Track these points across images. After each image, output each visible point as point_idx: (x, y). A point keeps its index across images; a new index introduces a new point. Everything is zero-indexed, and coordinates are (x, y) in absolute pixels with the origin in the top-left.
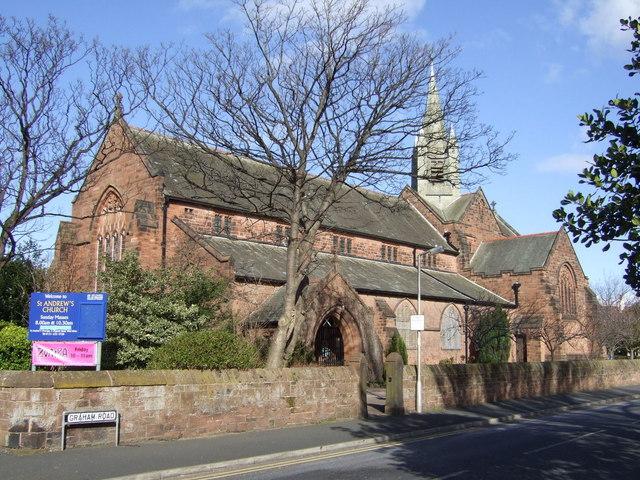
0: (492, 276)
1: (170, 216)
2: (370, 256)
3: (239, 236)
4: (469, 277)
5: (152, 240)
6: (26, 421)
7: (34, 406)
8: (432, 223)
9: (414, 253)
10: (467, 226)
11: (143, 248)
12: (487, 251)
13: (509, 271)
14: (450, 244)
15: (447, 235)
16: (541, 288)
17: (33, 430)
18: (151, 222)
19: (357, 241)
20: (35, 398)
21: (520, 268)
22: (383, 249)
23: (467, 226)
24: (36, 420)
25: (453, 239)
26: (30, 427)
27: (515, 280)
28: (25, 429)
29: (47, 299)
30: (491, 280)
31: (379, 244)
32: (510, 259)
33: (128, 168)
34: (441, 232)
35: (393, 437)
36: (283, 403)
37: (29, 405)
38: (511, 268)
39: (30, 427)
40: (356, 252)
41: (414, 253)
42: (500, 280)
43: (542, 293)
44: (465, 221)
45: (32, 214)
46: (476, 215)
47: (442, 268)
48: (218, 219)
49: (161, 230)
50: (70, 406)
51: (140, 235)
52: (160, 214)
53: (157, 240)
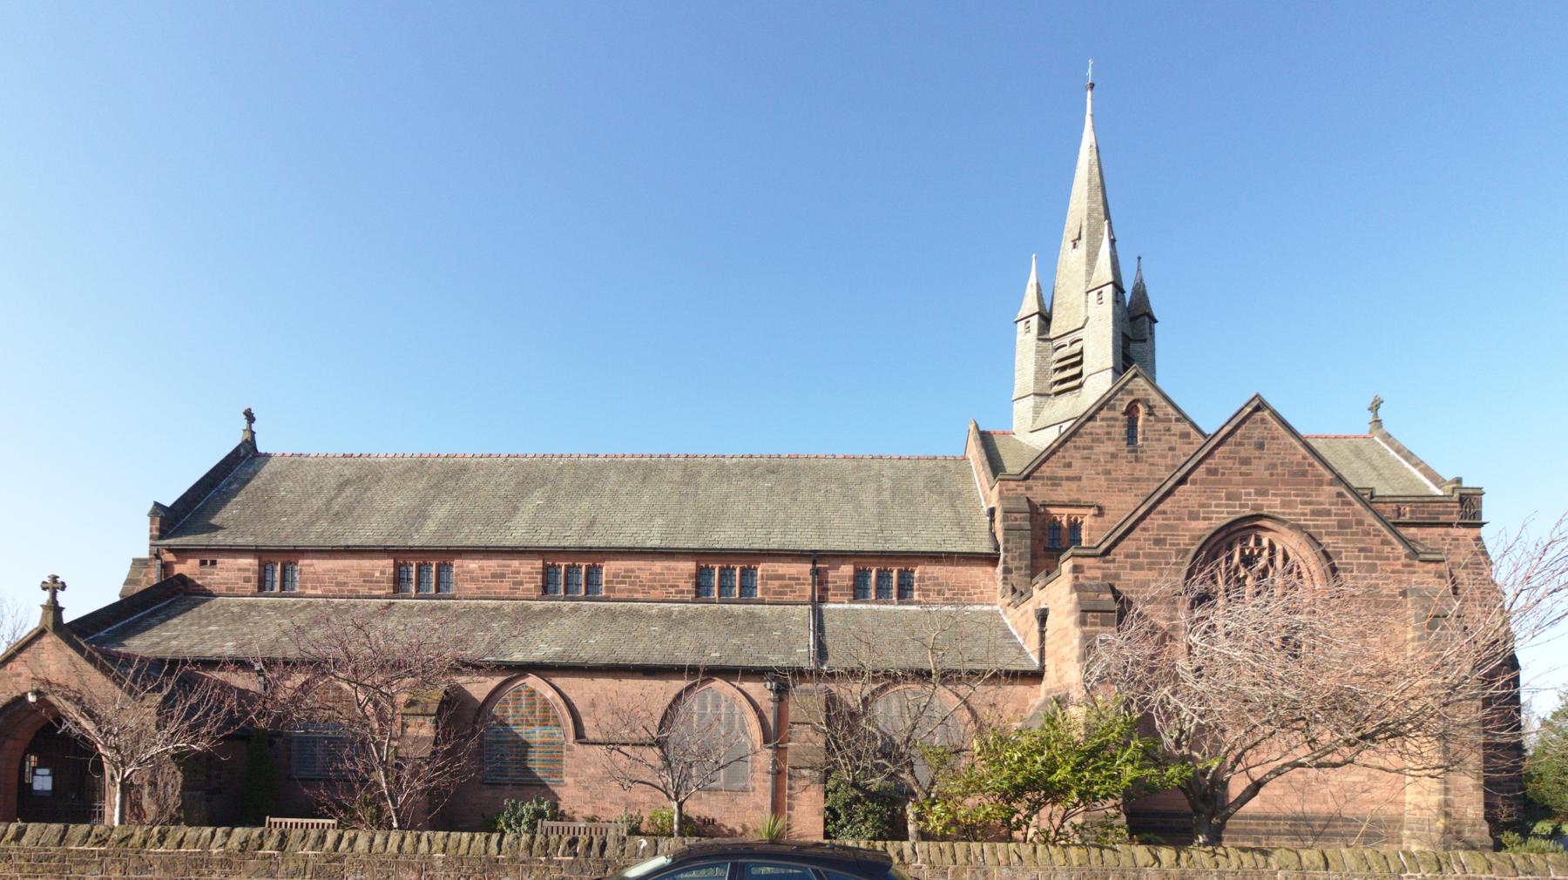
2: (654, 594)
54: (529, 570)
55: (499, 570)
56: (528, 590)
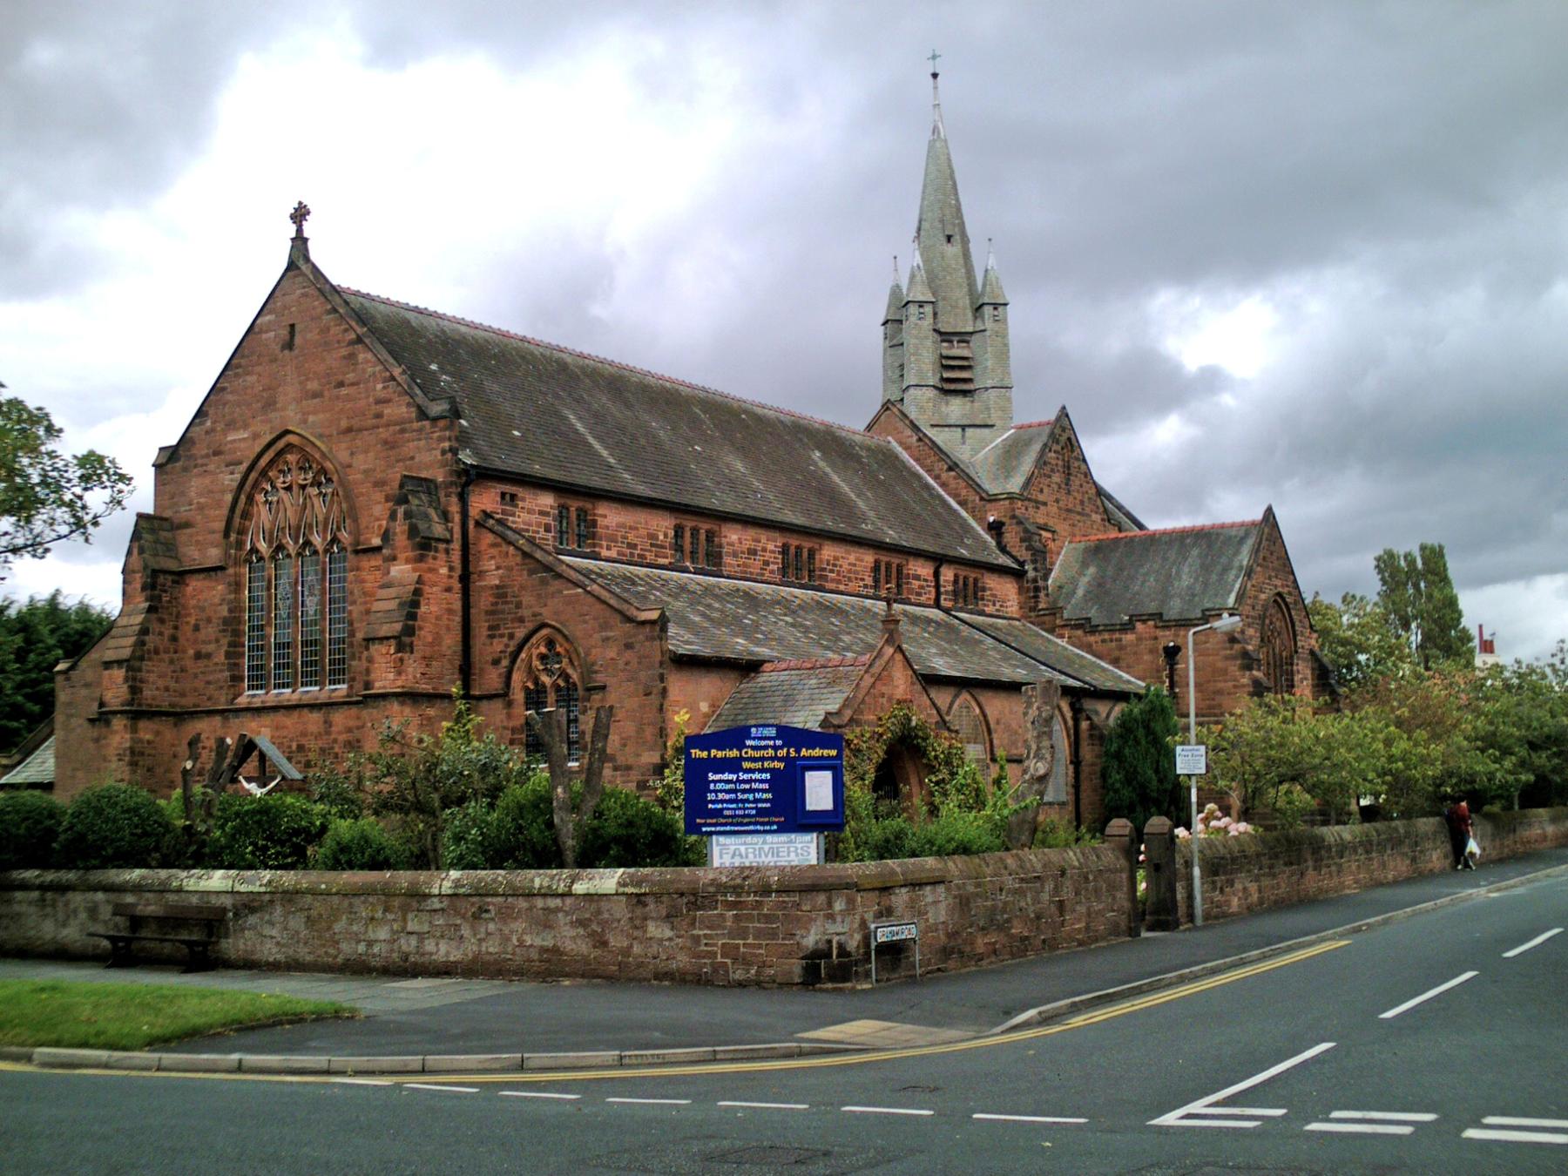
0: (1110, 628)
1: (474, 512)
2: (852, 586)
3: (605, 553)
4: (1051, 631)
5: (444, 571)
6: (829, 942)
7: (839, 919)
8: (955, 496)
9: (937, 574)
10: (1038, 504)
11: (426, 589)
12: (1085, 565)
13: (1152, 616)
14: (1003, 549)
15: (996, 528)
16: (1227, 658)
17: (839, 956)
18: (438, 530)
19: (828, 552)
20: (839, 905)
21: (1174, 609)
22: (877, 563)
23: (1038, 504)
24: (843, 938)
25: (1011, 536)
26: (835, 952)
27: (1168, 639)
28: (828, 955)
29: (780, 759)
30: (1106, 636)
31: (869, 558)
32: (1145, 587)
33: (344, 391)
34: (980, 520)
35: (1470, 903)
36: (1053, 908)
37: (831, 917)
38: (1152, 607)
39: (835, 952)
40: (824, 578)
41: (937, 574)
42: (1129, 638)
43: (1234, 668)
44: (1035, 495)
45: (1078, 684)
46: (1056, 478)
47: (990, 609)
48: (563, 508)
49: (456, 545)
50: (869, 916)
51: (421, 559)
52: (455, 509)
53: (451, 569)
54: (773, 548)
55: (753, 545)
56: (772, 572)
